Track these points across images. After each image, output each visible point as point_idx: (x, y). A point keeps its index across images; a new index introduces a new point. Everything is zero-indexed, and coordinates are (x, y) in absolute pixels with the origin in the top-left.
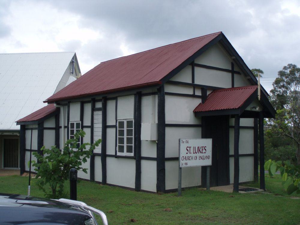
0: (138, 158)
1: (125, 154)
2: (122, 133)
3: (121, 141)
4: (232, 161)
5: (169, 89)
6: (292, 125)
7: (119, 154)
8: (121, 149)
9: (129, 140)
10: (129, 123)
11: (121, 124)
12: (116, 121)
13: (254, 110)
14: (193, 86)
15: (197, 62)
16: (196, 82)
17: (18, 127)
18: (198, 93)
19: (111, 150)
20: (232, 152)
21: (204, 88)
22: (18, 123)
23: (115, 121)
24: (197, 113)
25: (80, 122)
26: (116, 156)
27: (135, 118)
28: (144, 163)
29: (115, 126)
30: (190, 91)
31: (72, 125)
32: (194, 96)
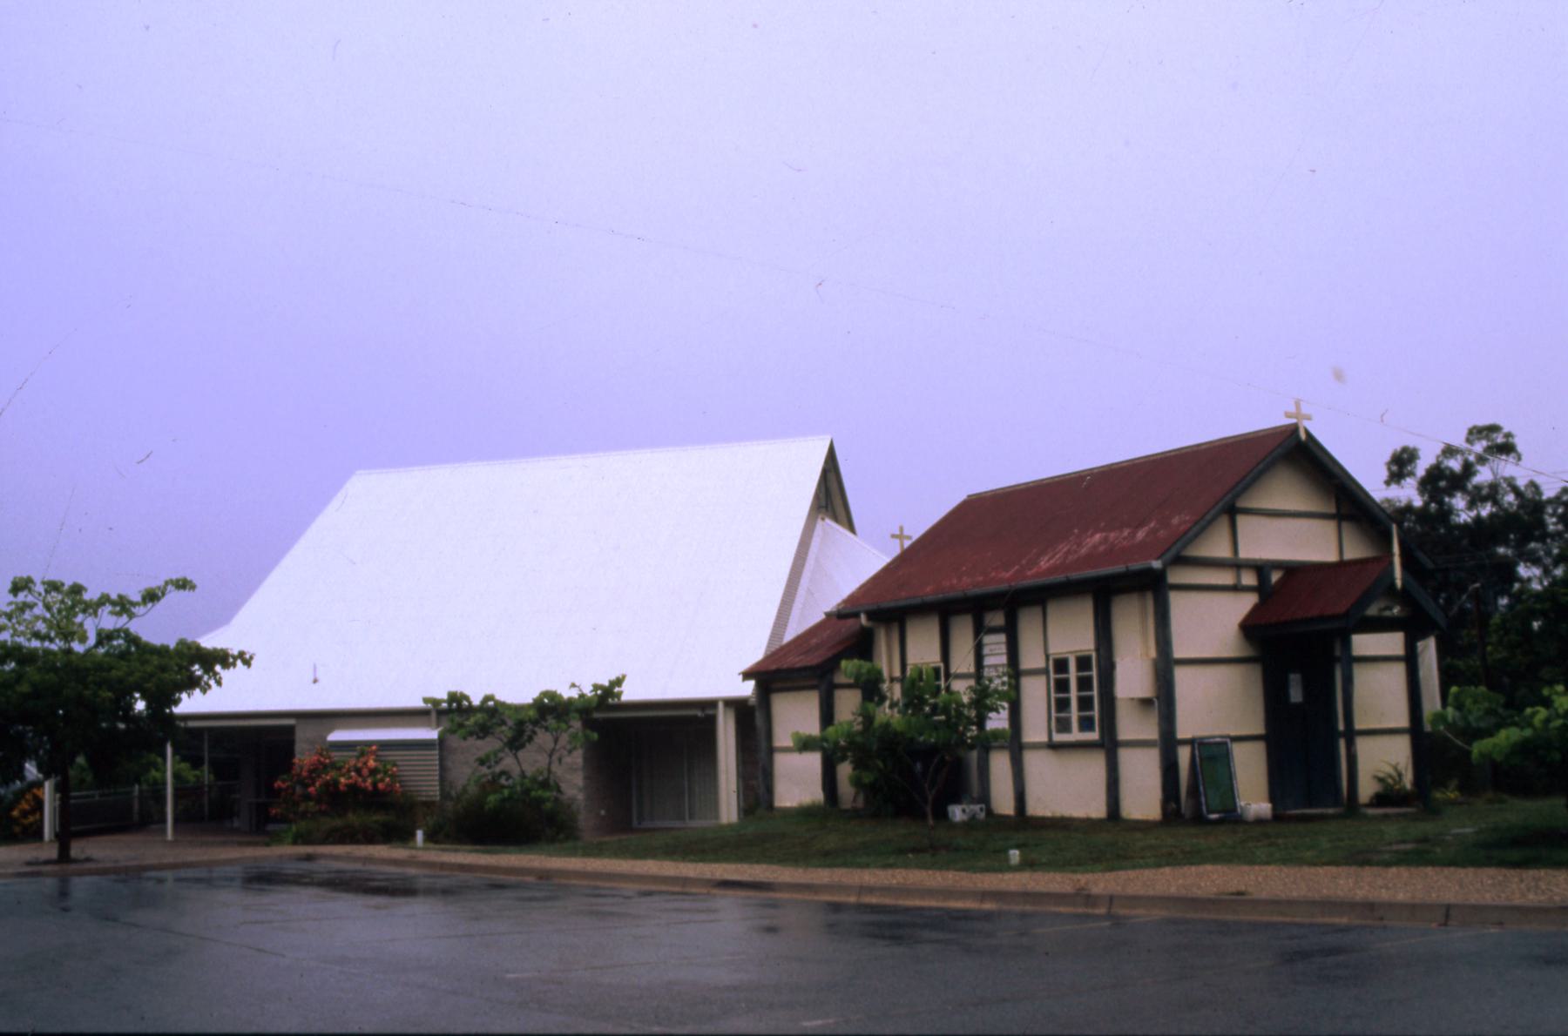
0: (1110, 745)
1: (1076, 735)
2: (1062, 686)
3: (1063, 705)
4: (1342, 744)
5: (1177, 576)
6: (1478, 663)
7: (1059, 738)
8: (1064, 726)
9: (1085, 703)
10: (1083, 663)
11: (1061, 665)
12: (1047, 657)
13: (1387, 613)
14: (1237, 565)
15: (1242, 503)
16: (1243, 554)
17: (747, 689)
18: (1249, 579)
19: (1036, 728)
20: (1341, 727)
21: (1261, 569)
22: (747, 675)
23: (1044, 657)
24: (1249, 628)
25: (942, 665)
26: (1053, 746)
27: (1097, 650)
28: (1125, 755)
29: (1045, 671)
30: (1226, 578)
31: (1061, 665)
32: (1236, 588)
